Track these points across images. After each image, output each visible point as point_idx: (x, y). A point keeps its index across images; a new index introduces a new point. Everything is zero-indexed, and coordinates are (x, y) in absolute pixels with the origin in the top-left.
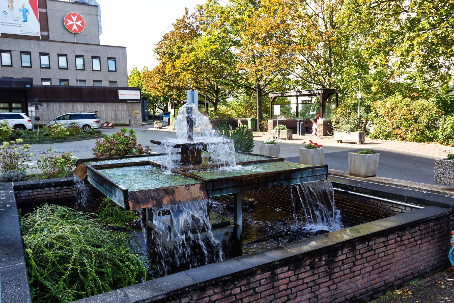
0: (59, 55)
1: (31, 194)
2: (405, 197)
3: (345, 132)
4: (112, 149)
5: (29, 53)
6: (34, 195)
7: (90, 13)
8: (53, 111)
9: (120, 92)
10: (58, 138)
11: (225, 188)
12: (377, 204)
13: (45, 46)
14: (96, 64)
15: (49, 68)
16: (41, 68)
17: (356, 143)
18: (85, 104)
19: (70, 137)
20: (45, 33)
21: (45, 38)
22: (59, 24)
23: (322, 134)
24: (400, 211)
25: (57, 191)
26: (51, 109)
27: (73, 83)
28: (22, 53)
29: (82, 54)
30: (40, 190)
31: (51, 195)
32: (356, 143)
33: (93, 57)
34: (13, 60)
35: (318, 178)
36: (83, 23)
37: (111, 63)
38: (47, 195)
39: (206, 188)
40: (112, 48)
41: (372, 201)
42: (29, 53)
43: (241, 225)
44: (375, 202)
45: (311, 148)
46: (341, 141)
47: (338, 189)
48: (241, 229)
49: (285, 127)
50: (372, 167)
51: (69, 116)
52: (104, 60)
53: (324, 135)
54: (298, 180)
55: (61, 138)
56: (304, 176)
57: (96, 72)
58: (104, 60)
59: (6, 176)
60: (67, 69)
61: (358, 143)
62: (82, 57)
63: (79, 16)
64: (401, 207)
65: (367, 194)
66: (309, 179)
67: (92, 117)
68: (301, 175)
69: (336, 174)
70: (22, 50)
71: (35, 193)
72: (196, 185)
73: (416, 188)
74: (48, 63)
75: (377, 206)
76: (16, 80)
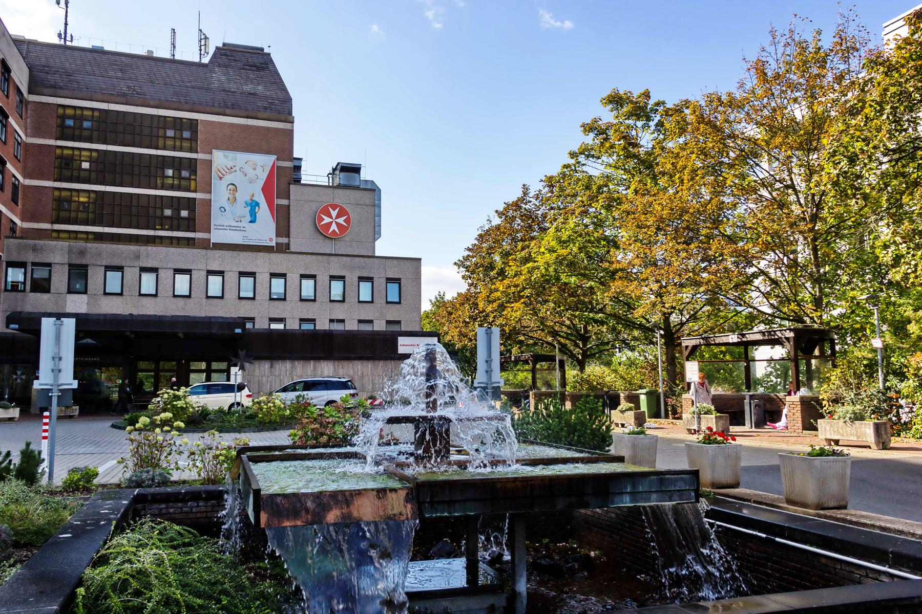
0: (303, 276)
1: (164, 511)
2: (887, 553)
3: (842, 420)
4: (322, 434)
5: (252, 274)
6: (170, 513)
7: (361, 202)
8: (280, 375)
9: (401, 340)
10: (270, 422)
11: (459, 501)
12: (835, 569)
13: (279, 262)
14: (365, 291)
15: (284, 299)
16: (271, 299)
17: (870, 447)
18: (336, 363)
19: (289, 421)
20: (284, 240)
21: (283, 249)
22: (308, 225)
23: (800, 424)
25: (210, 509)
26: (277, 373)
27: (323, 325)
28: (242, 274)
29: (343, 274)
30: (180, 505)
31: (199, 515)
32: (870, 447)
33: (361, 279)
34: (226, 287)
35: (675, 497)
36: (347, 221)
37: (393, 288)
38: (191, 516)
39: (418, 496)
40: (395, 262)
41: (823, 560)
42: (252, 274)
43: (525, 594)
44: (830, 563)
45: (709, 443)
47: (755, 533)
48: (525, 602)
49: (713, 408)
50: (833, 487)
51: (302, 384)
52: (380, 282)
53: (804, 428)
54: (627, 498)
55: (275, 422)
56: (641, 489)
57: (365, 305)
58: (380, 282)
59: (134, 478)
60: (314, 300)
61: (874, 446)
62: (342, 278)
63: (341, 208)
65: (811, 545)
66: (654, 496)
67: (344, 386)
68: (634, 486)
69: (760, 500)
70: (241, 270)
71: (171, 510)
72: (400, 492)
74: (282, 291)
75: (836, 574)
76: (220, 320)
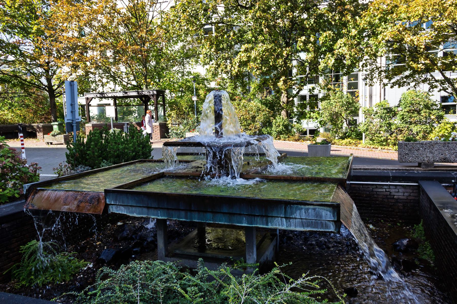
23: (159, 136)
24: (384, 190)
44: (356, 186)
46: (51, 143)
64: (385, 187)
73: (384, 169)
